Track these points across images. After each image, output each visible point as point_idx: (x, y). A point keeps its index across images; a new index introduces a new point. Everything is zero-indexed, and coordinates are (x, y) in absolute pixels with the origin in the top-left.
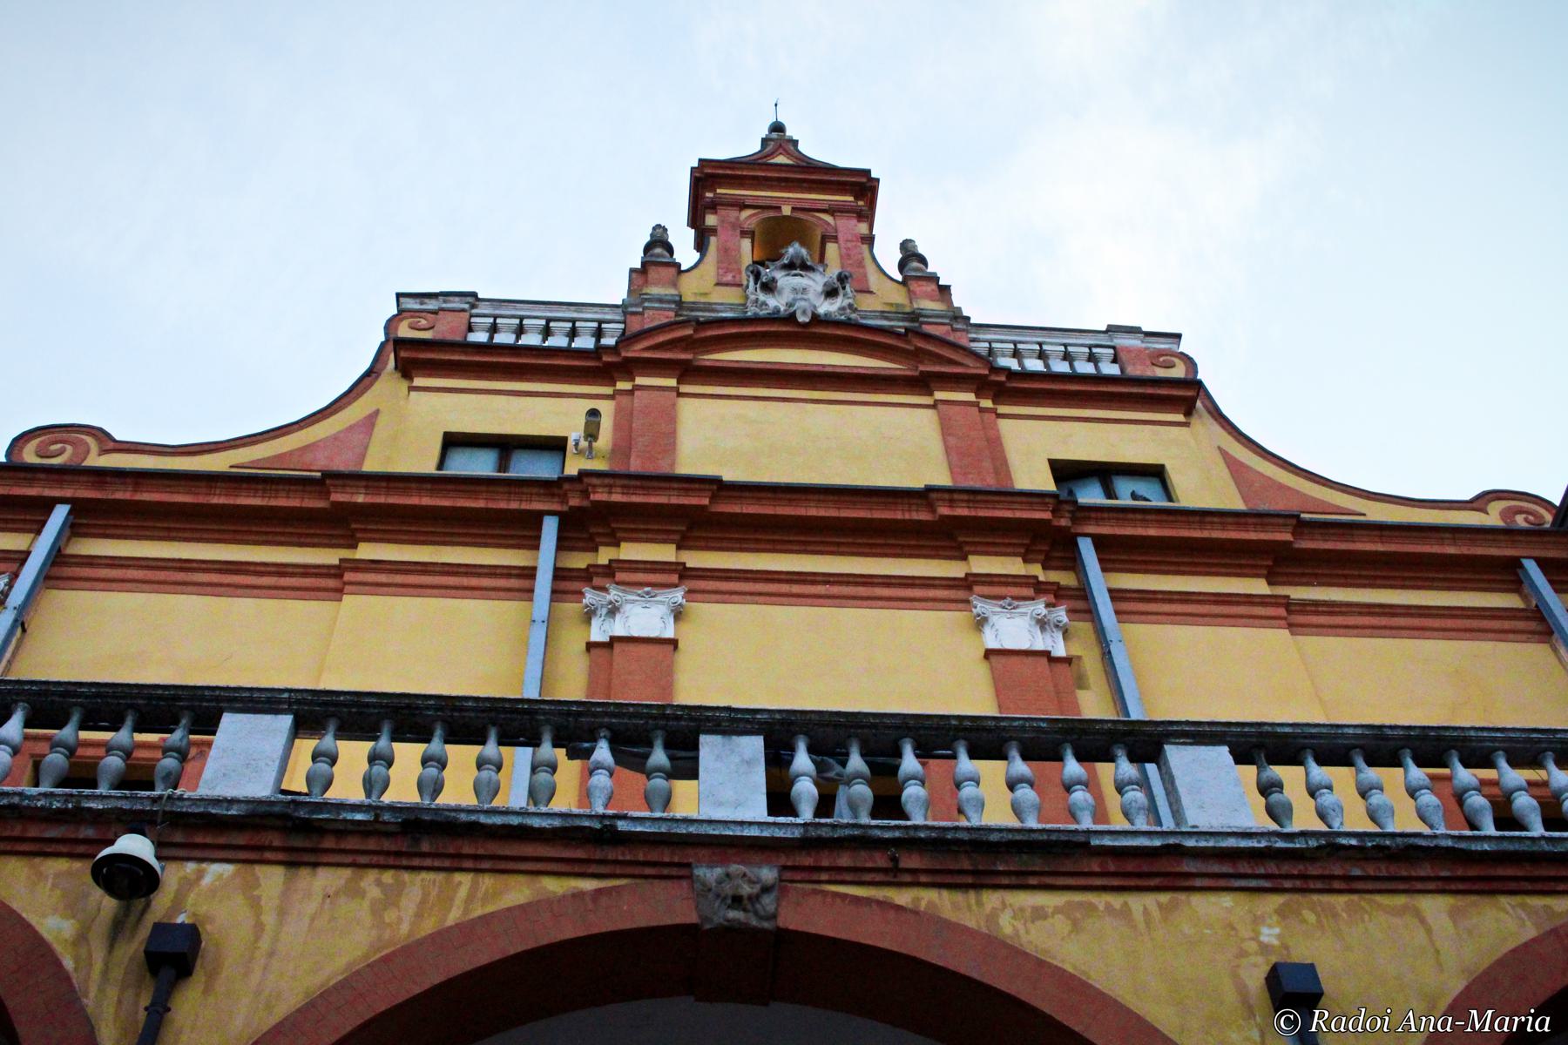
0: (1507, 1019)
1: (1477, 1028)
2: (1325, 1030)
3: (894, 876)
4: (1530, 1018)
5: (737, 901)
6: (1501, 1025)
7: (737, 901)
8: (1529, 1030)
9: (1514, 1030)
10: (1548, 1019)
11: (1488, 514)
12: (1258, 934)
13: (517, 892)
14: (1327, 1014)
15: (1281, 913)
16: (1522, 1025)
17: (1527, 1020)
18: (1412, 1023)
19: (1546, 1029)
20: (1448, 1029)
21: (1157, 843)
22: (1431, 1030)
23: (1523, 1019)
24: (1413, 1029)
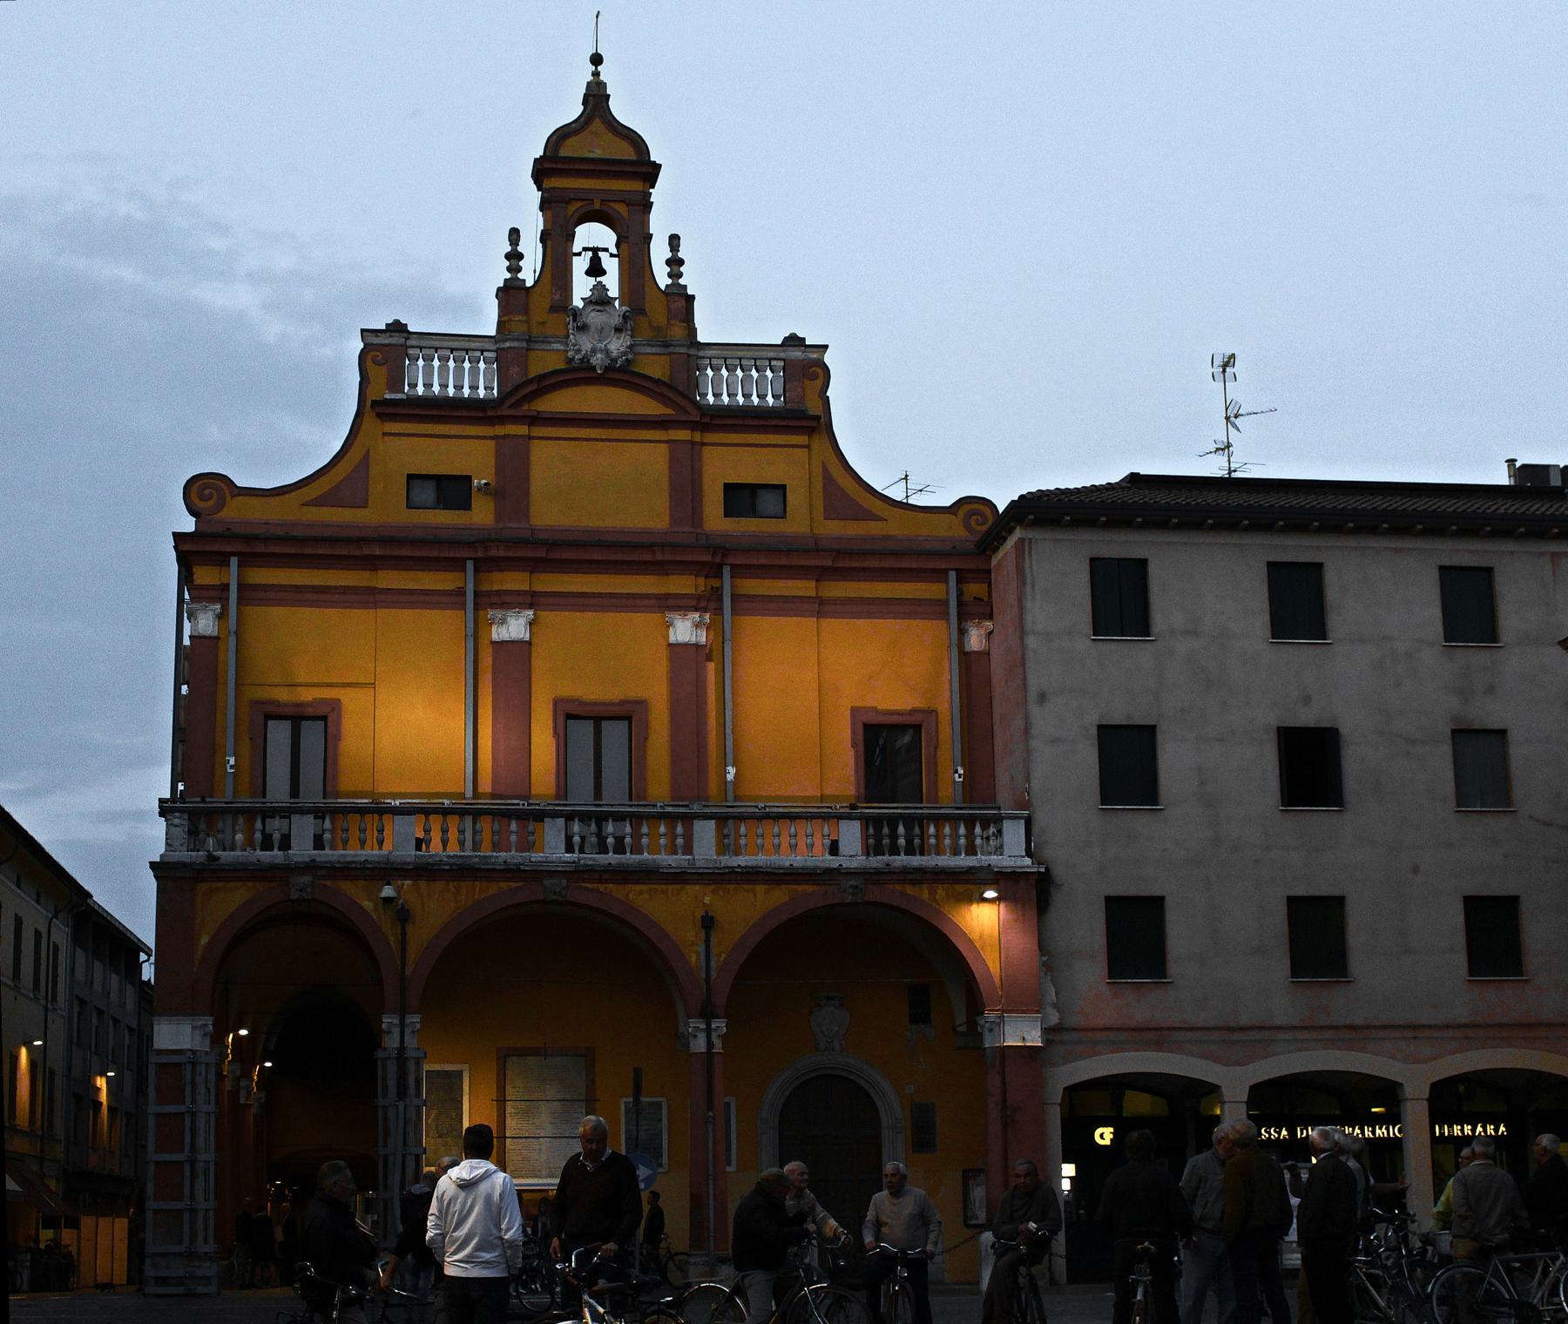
3: (601, 881)
5: (555, 893)
13: (493, 889)
15: (713, 892)
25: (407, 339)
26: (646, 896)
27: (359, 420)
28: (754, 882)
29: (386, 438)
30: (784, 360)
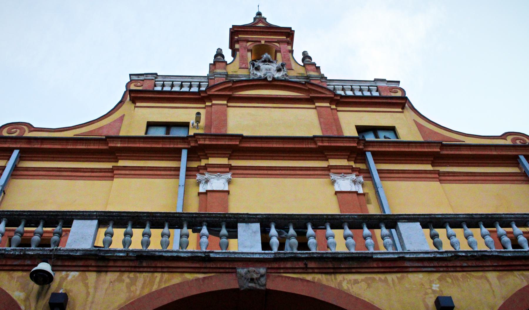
3: (306, 270)
5: (252, 280)
11: (507, 140)
12: (432, 286)
13: (176, 279)
15: (440, 279)
21: (396, 256)
25: (156, 78)
26: (363, 285)
27: (120, 104)
28: (484, 269)
29: (136, 109)
30: (377, 86)
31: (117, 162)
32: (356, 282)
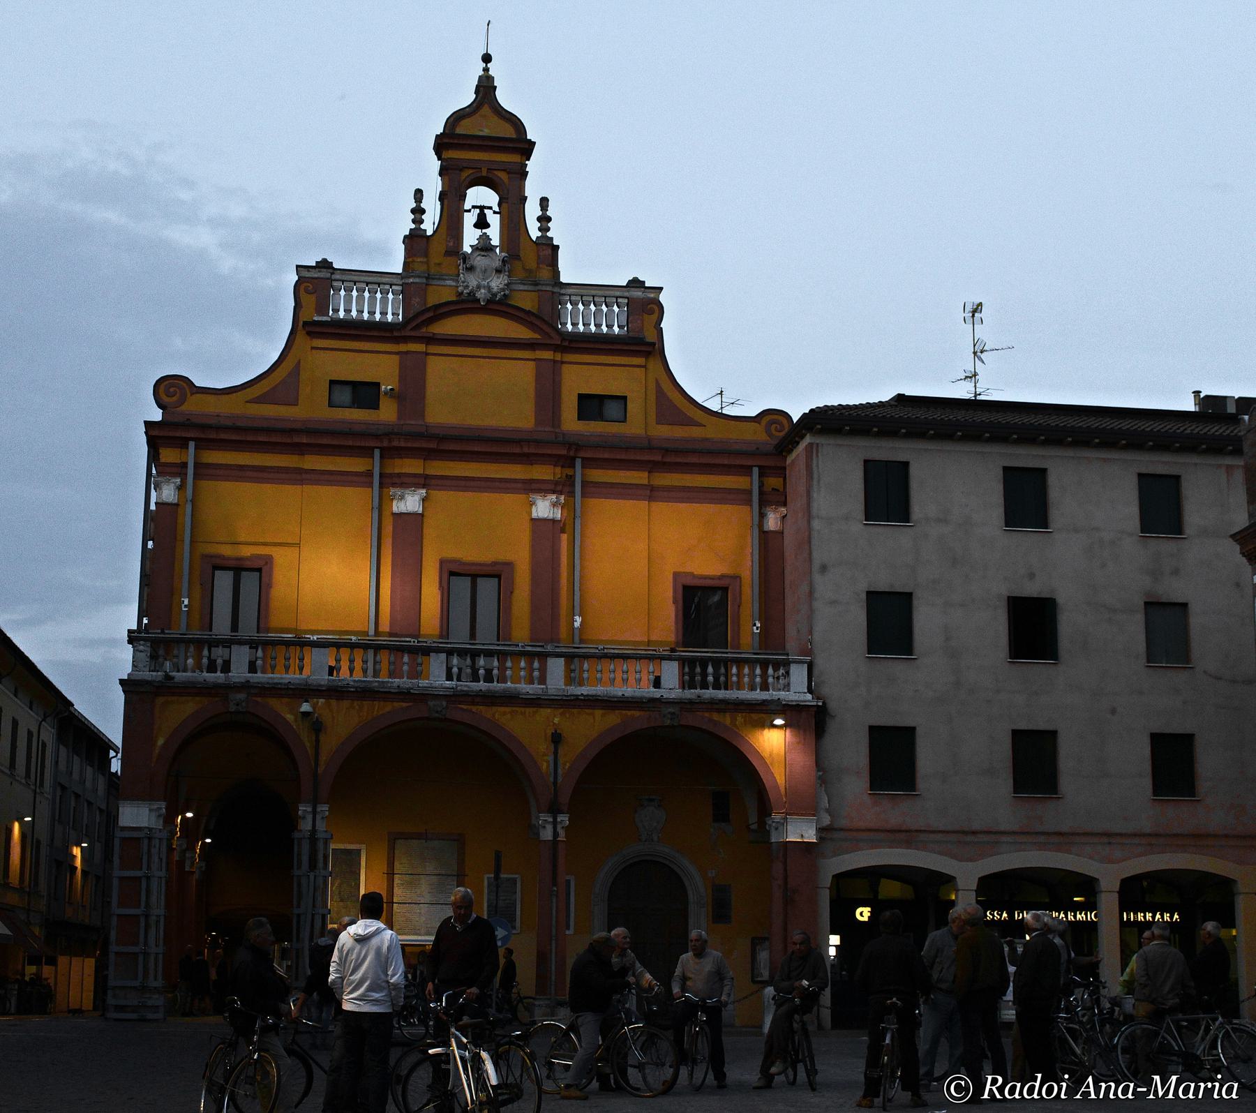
0: (1193, 1085)
1: (1160, 1095)
2: (998, 1096)
3: (473, 703)
4: (1217, 1085)
5: (437, 712)
6: (1186, 1091)
7: (437, 712)
8: (1216, 1096)
9: (1200, 1097)
10: (1236, 1085)
11: (13, 718)
12: (554, 719)
13: (388, 707)
14: (1000, 1080)
15: (561, 714)
16: (1208, 1092)
17: (1214, 1087)
18: (1092, 1089)
19: (1234, 1096)
20: (1130, 1096)
21: (535, 697)
22: (1111, 1096)
23: (1210, 1085)
24: (1093, 1096)
26: (509, 716)
31: (77, 868)
32: (504, 713)
